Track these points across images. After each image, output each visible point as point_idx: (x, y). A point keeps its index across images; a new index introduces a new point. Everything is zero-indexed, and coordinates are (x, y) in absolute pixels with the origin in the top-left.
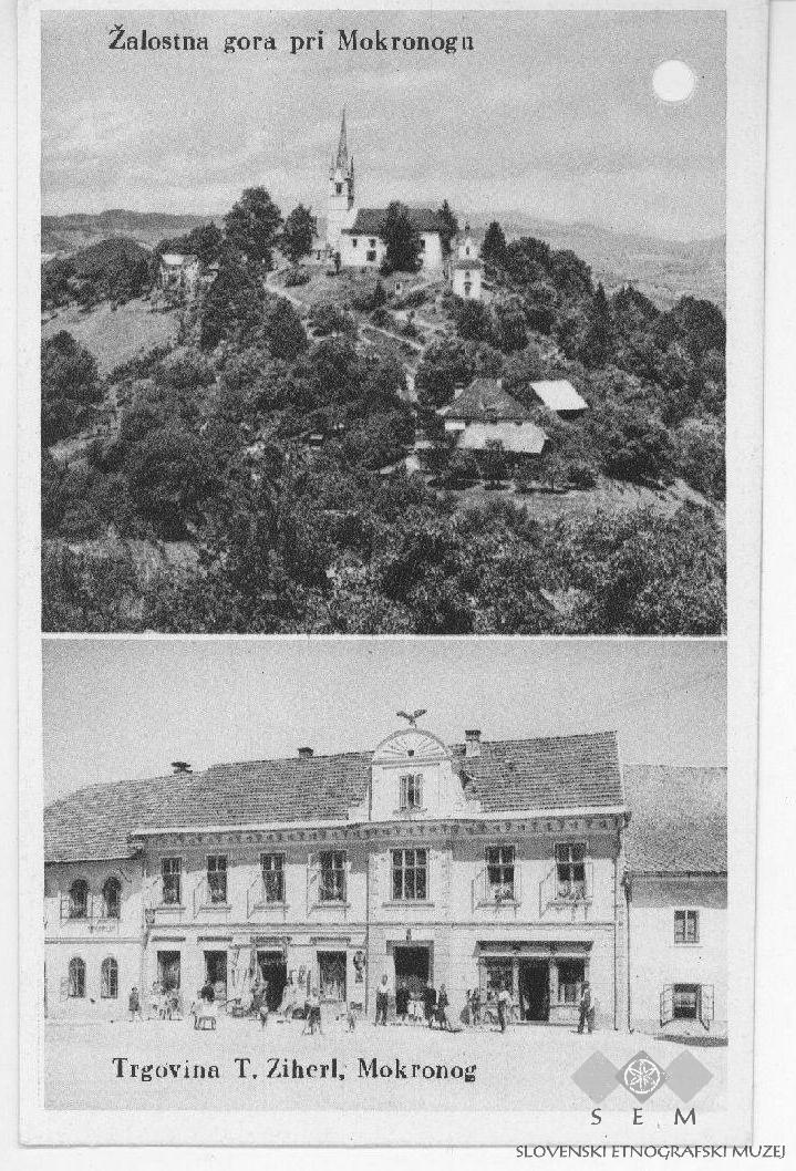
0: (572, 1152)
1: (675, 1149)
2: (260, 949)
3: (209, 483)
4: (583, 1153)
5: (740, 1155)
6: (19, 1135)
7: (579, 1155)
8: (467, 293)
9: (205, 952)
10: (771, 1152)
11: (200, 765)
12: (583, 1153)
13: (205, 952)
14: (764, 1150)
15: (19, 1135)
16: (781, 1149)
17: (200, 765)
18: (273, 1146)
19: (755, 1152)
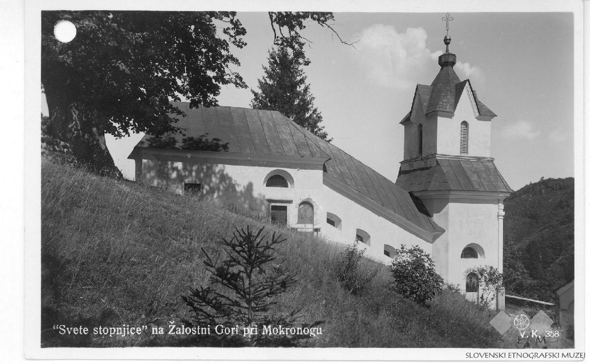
0: (493, 355)
1: (536, 354)
2: (507, 295)
3: (223, 309)
4: (495, 356)
5: (565, 357)
6: (25, 355)
7: (494, 357)
8: (561, 310)
9: (328, 213)
10: (579, 356)
11: (182, 95)
12: (495, 356)
13: (328, 213)
14: (576, 355)
15: (25, 355)
16: (583, 354)
17: (182, 95)
18: (273, 360)
19: (572, 356)
